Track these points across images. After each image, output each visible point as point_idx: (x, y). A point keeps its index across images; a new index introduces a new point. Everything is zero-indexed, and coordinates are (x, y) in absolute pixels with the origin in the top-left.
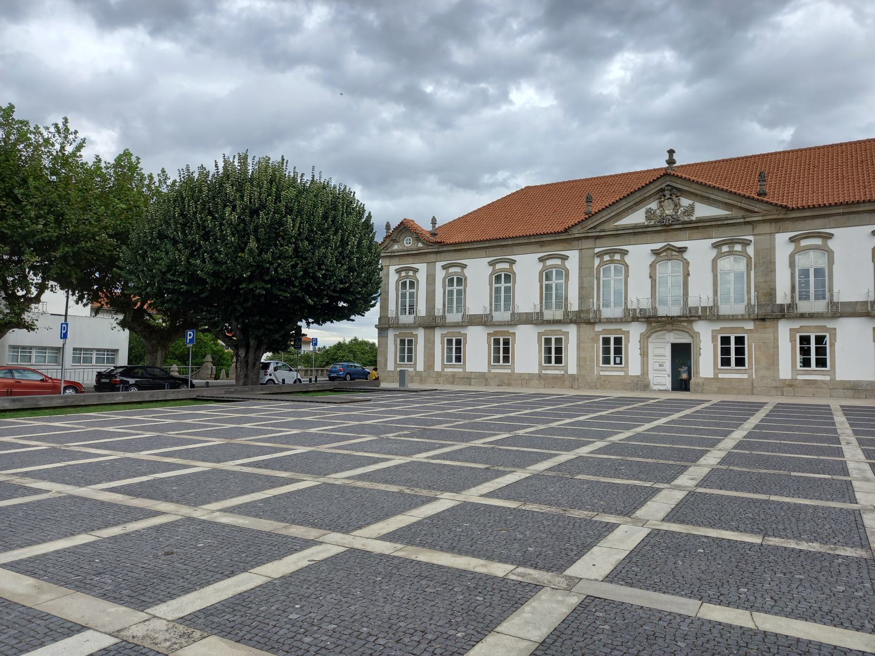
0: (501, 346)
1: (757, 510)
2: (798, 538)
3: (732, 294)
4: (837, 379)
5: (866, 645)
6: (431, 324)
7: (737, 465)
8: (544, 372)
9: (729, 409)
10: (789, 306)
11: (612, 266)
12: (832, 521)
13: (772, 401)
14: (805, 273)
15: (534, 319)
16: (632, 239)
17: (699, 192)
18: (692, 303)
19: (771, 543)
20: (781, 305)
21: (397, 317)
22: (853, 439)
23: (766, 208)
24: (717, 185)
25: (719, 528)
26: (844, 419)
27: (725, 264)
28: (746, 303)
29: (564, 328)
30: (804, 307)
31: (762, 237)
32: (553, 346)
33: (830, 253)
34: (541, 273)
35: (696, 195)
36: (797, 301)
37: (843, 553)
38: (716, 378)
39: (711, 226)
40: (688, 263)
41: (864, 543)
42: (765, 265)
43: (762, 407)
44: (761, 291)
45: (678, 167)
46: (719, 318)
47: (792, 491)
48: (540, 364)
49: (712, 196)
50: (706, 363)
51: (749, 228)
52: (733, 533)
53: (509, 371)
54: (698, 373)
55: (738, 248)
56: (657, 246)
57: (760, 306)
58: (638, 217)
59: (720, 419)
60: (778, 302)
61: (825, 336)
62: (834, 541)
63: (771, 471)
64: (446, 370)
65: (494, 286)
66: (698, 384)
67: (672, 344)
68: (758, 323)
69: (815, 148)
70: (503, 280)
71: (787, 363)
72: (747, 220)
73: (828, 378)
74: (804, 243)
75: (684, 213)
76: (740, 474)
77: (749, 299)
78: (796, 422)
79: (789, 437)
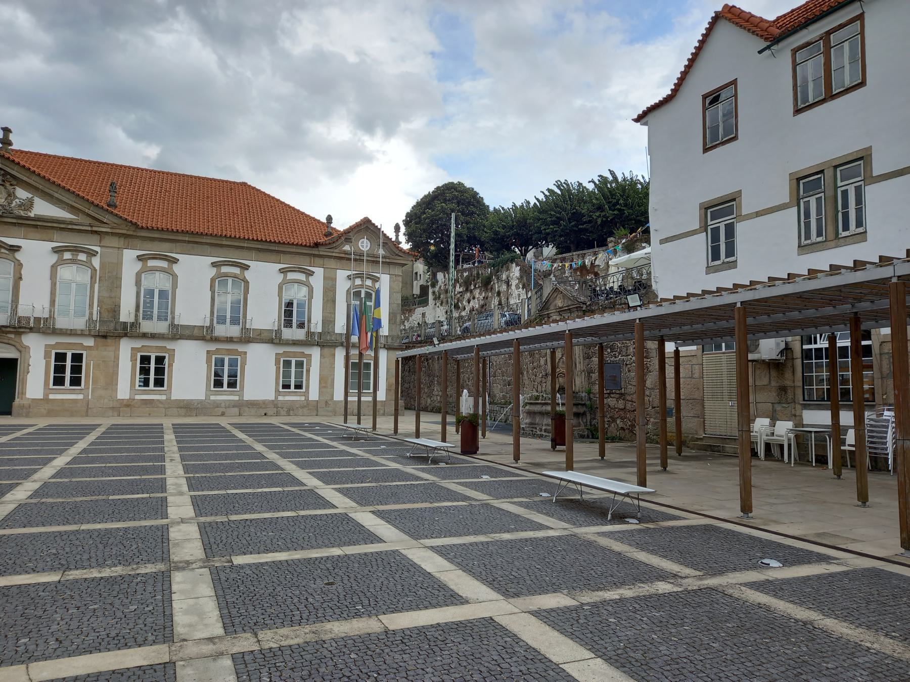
1: (62, 544)
2: (101, 565)
3: (72, 307)
5: (144, 659)
7: (51, 496)
9: (56, 434)
10: (132, 324)
12: (140, 541)
13: (106, 422)
14: (150, 293)
15: (203, 335)
17: (41, 187)
18: (21, 313)
19: (71, 577)
20: (125, 323)
22: (177, 456)
23: (116, 221)
24: (63, 184)
25: (10, 574)
26: (173, 437)
27: (66, 273)
28: (169, 322)
29: (307, 351)
30: (147, 326)
31: (110, 250)
33: (175, 277)
35: (37, 189)
36: (141, 320)
37: (142, 571)
38: (46, 400)
39: (52, 228)
40: (21, 265)
41: (165, 556)
42: (110, 279)
43: (94, 429)
44: (104, 307)
45: (13, 150)
46: (55, 332)
47: (106, 516)
48: (277, 391)
49: (56, 195)
51: (96, 238)
52: (28, 576)
54: (24, 393)
55: (82, 257)
59: (212, 436)
60: (121, 320)
61: (164, 357)
62: (137, 560)
63: (88, 498)
66: (22, 407)
67: (17, 360)
68: (98, 339)
69: (168, 173)
71: (126, 383)
72: (95, 229)
73: (164, 397)
74: (151, 263)
75: (20, 206)
76: (52, 505)
77: (91, 314)
78: (126, 443)
79: (116, 459)
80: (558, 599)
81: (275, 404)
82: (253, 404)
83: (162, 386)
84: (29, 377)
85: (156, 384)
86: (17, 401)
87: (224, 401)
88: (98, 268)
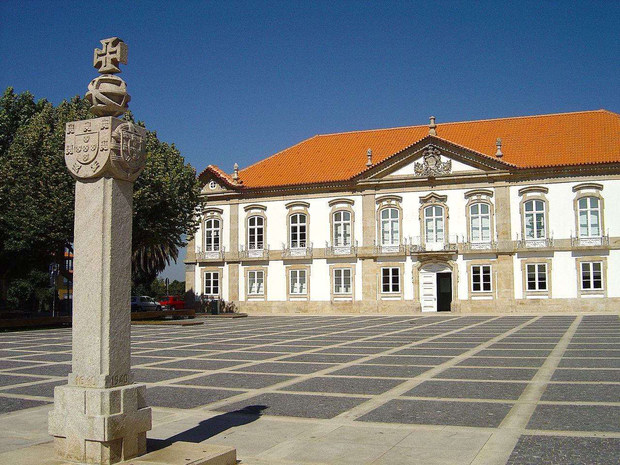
8: (335, 299)
11: (390, 209)
16: (405, 189)
34: (331, 215)
38: (470, 301)
48: (579, 290)
50: (462, 288)
56: (424, 194)
58: (408, 171)
65: (249, 227)
67: (451, 273)
70: (536, 212)
86: (452, 303)
88: (494, 203)
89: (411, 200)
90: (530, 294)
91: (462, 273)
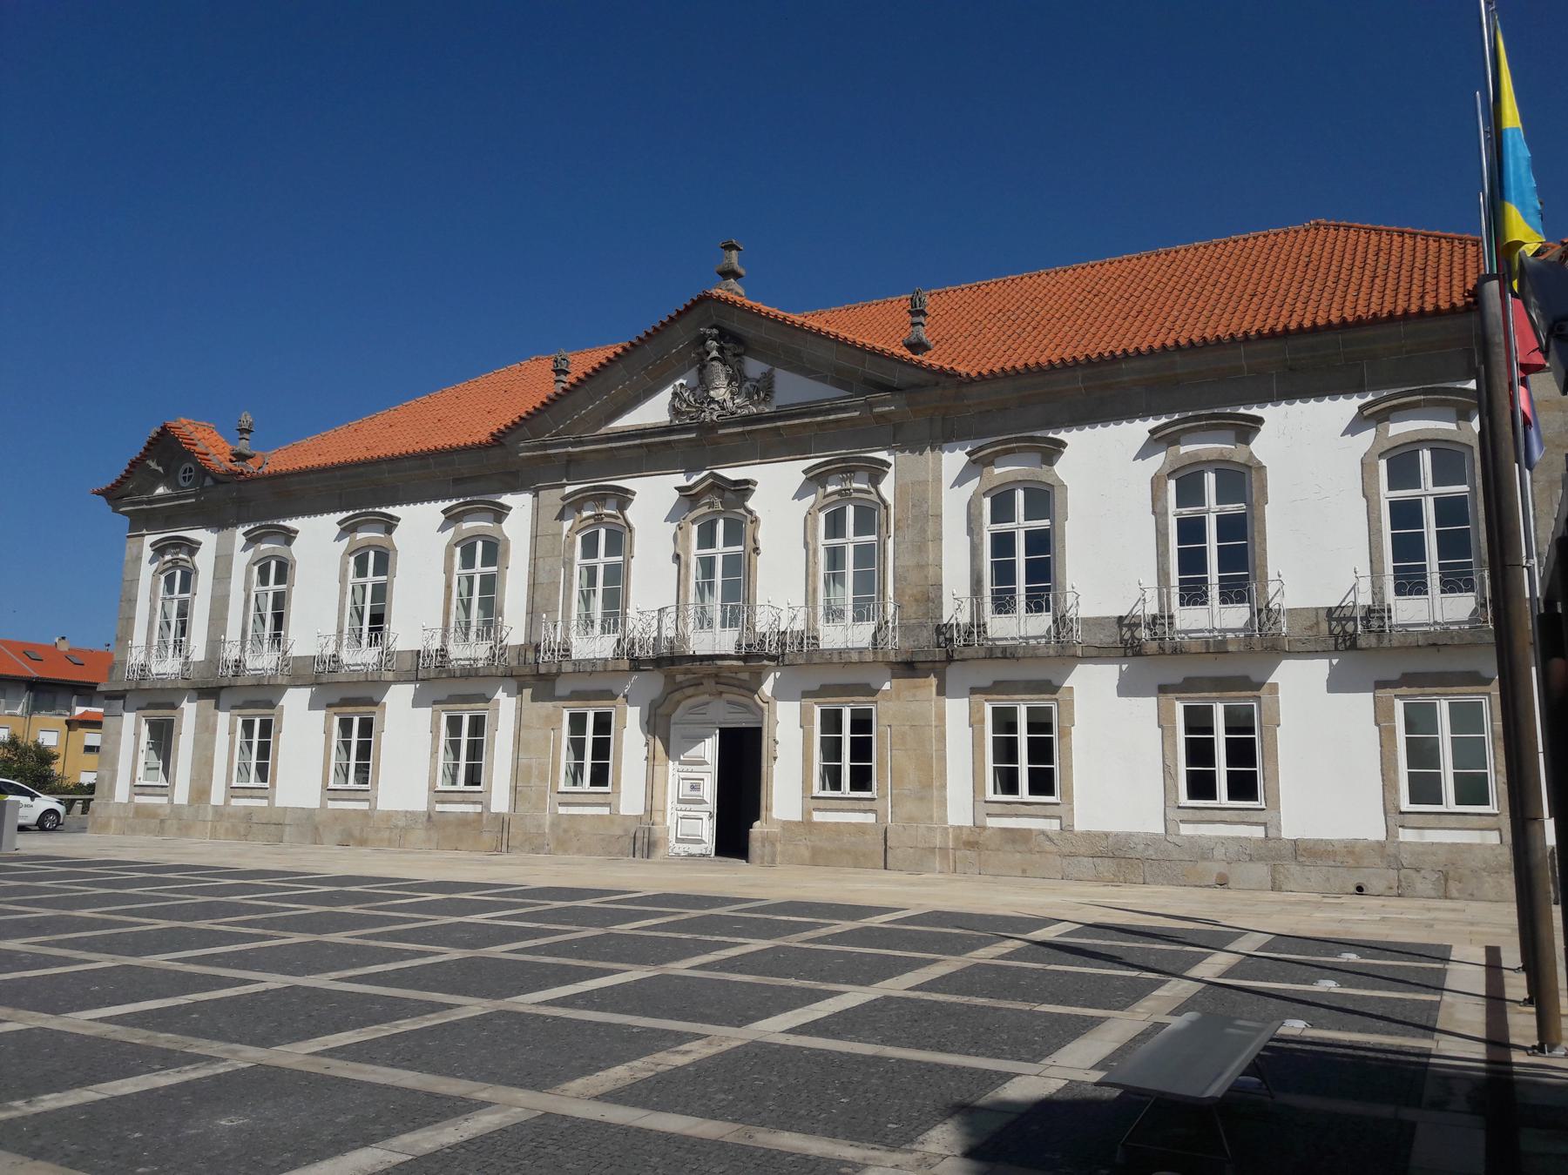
0: (846, 735)
4: (1079, 827)
6: (935, 657)
8: (439, 808)
15: (1133, 646)
21: (978, 626)
32: (1220, 737)
36: (1390, 596)
38: (807, 824)
48: (1391, 810)
53: (364, 806)
57: (905, 629)
58: (654, 411)
64: (234, 802)
66: (767, 839)
80: (480, 1126)
81: (1386, 852)
82: (1308, 852)
83: (1252, 795)
84: (777, 767)
85: (1033, 790)
87: (1223, 841)
88: (890, 500)
89: (653, 496)
90: (997, 809)
91: (790, 736)
